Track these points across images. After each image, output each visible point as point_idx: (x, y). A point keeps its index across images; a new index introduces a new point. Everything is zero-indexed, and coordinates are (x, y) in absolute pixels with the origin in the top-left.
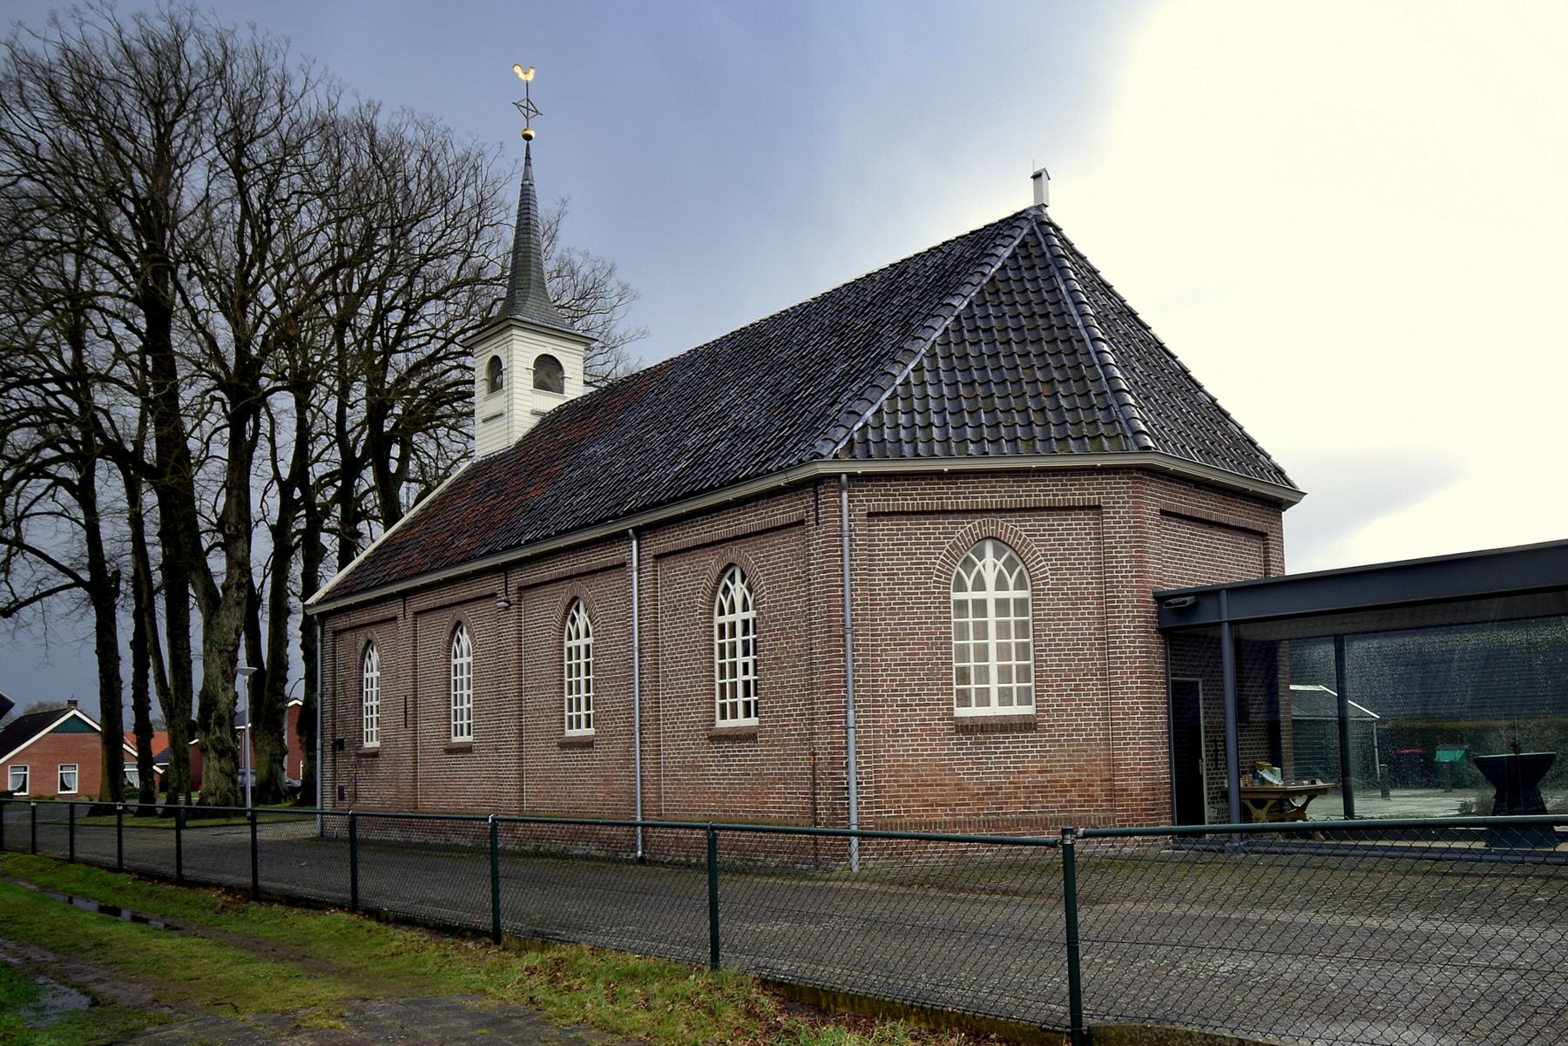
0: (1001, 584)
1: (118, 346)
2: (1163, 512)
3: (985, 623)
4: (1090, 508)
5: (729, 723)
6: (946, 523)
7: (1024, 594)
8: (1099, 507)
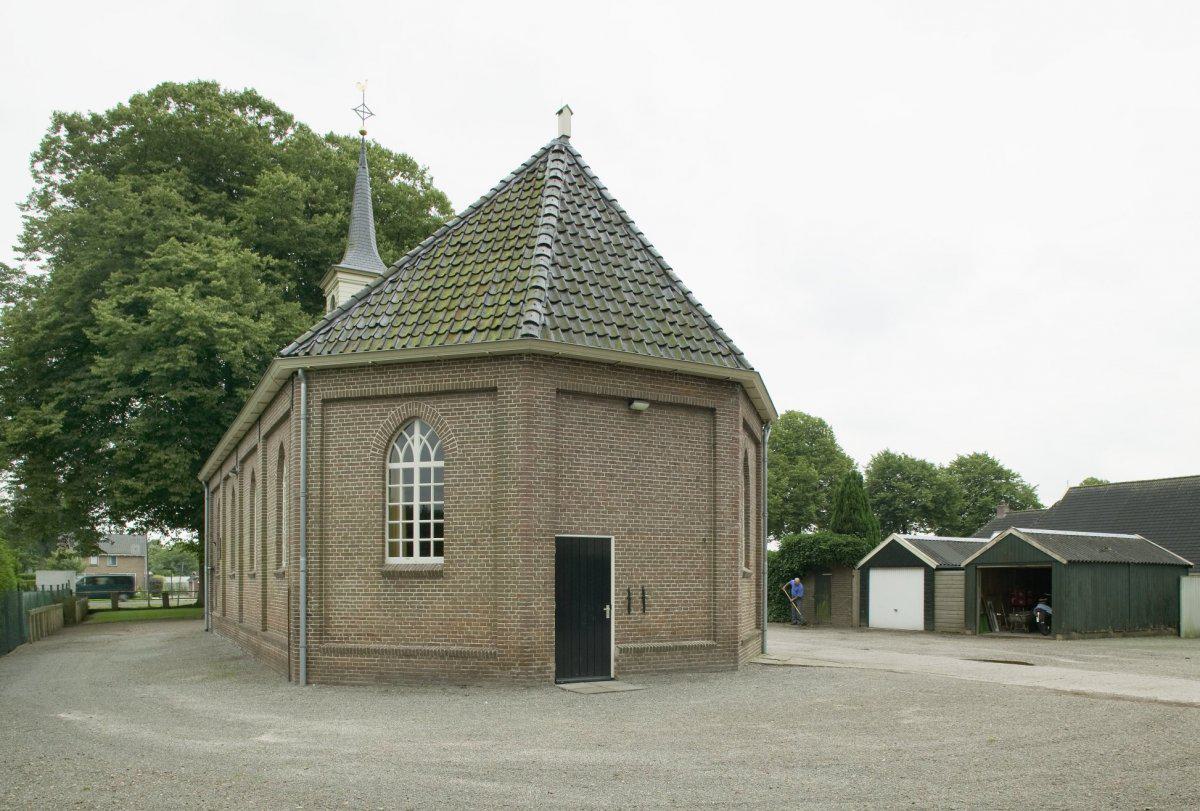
0: (425, 456)
1: (382, 327)
2: (558, 391)
3: (412, 524)
4: (623, 399)
5: (400, 561)
6: (381, 406)
7: (441, 464)
8: (495, 389)
